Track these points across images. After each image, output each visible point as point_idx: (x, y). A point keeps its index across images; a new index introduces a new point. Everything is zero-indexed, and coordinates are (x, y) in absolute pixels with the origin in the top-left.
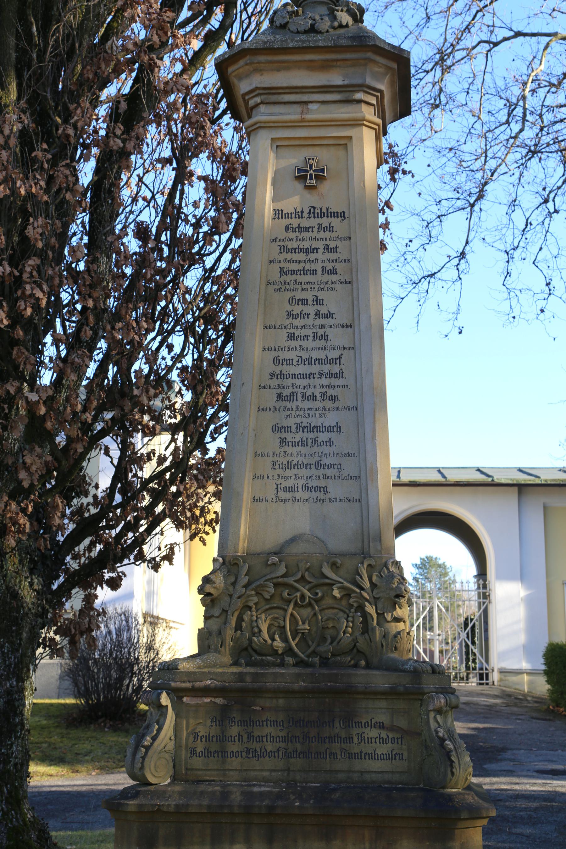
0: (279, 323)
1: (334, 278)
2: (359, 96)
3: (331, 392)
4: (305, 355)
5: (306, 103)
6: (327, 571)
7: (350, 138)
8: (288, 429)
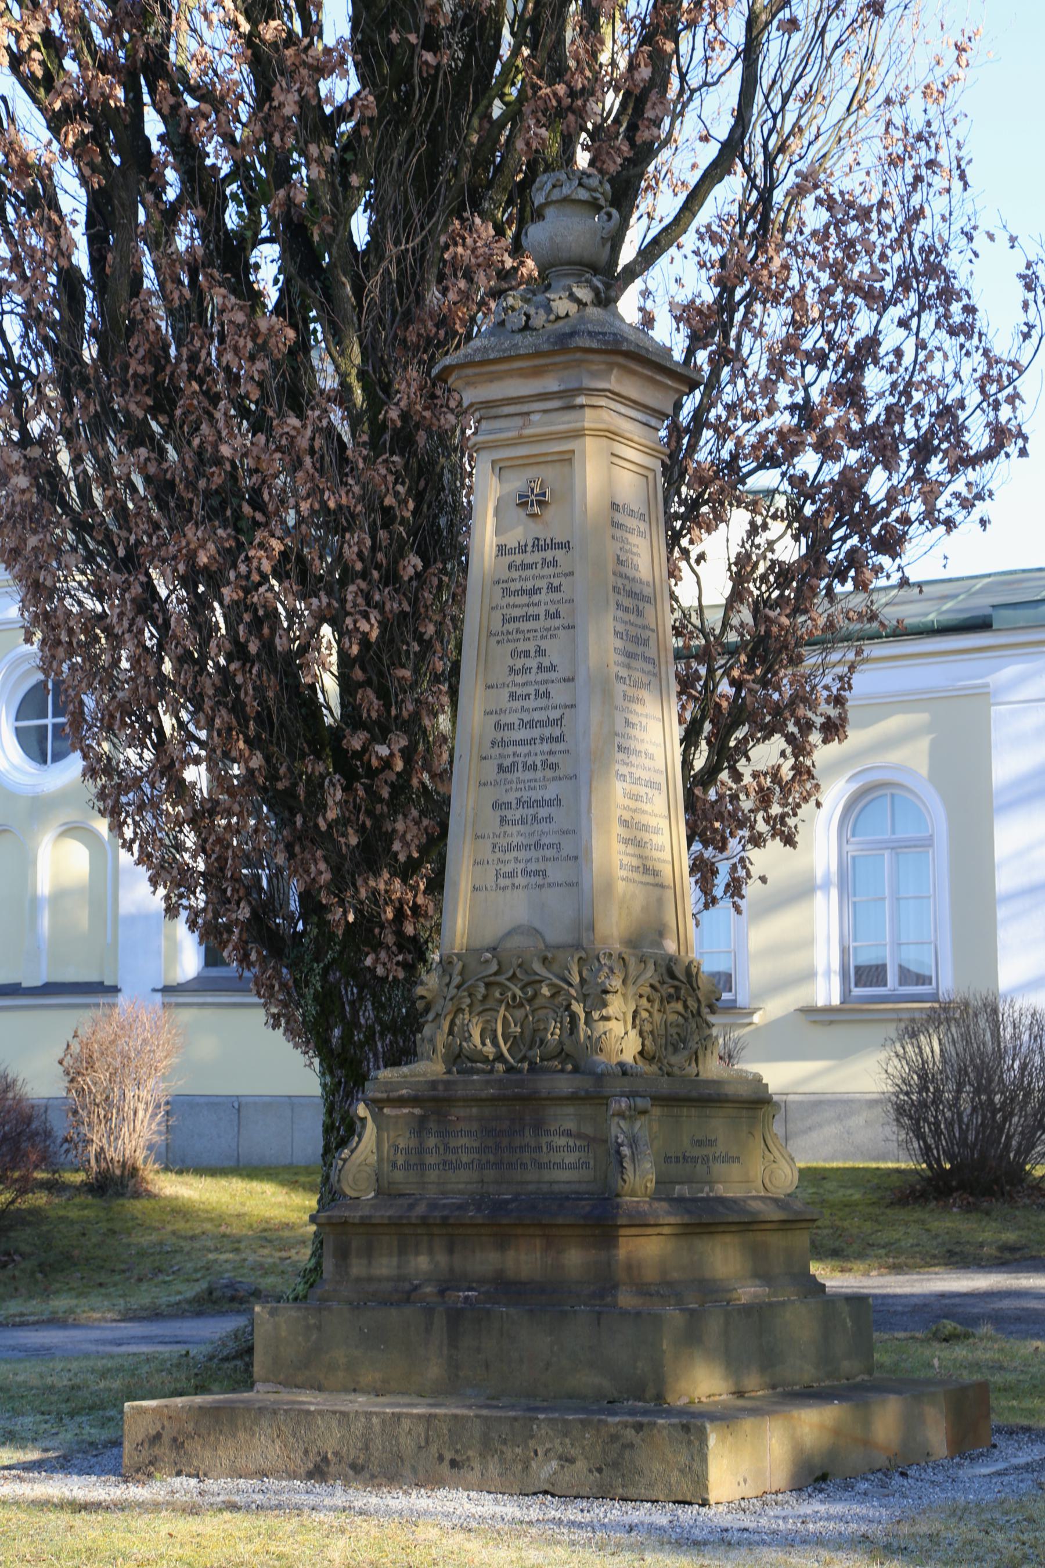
0: (500, 682)
1: (557, 622)
2: (581, 400)
3: (552, 759)
4: (526, 718)
5: (528, 414)
6: (537, 967)
7: (573, 452)
8: (508, 805)
